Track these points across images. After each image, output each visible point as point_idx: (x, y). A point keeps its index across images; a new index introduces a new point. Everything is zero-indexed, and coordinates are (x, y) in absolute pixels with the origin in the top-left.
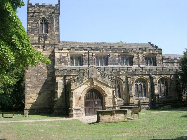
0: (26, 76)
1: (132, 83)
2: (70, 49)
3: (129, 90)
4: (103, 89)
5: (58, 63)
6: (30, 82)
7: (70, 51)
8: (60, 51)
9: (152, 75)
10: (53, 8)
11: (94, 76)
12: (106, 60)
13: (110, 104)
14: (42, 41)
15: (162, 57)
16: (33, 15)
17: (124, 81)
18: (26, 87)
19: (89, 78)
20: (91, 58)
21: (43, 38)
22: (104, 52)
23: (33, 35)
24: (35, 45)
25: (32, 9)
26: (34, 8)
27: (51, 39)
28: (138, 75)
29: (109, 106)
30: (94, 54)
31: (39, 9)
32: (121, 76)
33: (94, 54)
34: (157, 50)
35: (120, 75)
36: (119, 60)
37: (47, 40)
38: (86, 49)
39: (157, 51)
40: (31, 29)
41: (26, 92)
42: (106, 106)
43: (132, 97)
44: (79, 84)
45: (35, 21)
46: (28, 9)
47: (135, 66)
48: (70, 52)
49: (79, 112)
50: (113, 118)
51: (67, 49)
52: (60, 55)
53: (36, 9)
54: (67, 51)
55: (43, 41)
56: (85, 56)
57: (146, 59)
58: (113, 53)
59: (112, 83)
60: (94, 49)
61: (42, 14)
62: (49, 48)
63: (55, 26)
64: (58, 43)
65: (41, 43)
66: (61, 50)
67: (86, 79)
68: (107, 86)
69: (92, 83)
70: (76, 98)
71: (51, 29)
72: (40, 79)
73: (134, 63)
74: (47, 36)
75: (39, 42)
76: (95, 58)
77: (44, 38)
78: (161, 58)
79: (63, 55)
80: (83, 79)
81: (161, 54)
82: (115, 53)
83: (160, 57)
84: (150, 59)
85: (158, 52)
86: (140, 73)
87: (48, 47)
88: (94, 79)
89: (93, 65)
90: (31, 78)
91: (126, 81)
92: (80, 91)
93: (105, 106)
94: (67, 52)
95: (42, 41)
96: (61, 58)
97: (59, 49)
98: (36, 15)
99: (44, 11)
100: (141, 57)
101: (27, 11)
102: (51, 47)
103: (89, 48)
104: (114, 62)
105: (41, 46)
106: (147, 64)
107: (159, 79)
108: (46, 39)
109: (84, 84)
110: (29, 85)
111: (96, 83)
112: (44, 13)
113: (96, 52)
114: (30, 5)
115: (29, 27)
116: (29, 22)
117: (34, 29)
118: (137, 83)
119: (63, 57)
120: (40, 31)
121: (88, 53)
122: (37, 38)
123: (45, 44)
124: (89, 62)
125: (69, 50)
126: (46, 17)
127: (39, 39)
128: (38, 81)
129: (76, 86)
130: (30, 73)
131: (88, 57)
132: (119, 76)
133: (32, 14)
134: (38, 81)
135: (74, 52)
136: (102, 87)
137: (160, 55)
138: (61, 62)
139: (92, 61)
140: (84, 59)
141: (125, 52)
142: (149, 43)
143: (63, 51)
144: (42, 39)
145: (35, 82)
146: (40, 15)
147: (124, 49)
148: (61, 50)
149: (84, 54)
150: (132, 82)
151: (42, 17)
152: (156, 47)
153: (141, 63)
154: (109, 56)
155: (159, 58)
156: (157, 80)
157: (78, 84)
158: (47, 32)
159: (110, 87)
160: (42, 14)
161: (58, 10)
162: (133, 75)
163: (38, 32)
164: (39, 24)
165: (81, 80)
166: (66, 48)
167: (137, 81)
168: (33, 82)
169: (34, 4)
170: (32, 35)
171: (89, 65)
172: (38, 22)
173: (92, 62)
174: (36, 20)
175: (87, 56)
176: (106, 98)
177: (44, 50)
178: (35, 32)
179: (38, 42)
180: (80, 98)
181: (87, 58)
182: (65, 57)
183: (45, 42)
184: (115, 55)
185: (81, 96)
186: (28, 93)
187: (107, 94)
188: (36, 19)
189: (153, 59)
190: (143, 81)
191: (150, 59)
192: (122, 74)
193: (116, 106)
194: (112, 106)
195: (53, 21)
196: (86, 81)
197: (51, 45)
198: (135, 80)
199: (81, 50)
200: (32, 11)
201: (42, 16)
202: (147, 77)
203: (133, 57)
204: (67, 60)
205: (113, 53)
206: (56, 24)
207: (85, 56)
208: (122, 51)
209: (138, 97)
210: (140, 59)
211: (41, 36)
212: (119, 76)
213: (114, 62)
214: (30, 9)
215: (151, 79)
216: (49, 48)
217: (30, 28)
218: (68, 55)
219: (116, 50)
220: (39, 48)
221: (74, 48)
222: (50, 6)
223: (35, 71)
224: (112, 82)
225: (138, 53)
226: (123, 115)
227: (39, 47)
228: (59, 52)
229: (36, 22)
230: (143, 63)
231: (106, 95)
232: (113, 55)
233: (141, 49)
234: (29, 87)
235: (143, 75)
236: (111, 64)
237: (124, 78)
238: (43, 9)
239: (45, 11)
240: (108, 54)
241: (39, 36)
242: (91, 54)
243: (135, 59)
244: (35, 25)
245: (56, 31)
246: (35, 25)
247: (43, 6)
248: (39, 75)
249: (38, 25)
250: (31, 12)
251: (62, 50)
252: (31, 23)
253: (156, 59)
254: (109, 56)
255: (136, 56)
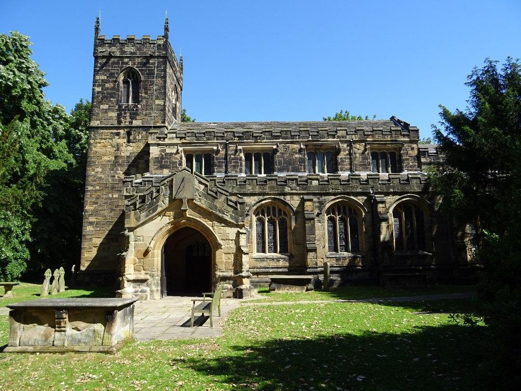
0: (86, 199)
1: (318, 215)
2: (184, 136)
3: (307, 232)
4: (211, 228)
5: (157, 169)
6: (95, 213)
7: (185, 141)
8: (160, 142)
9: (376, 193)
10: (152, 45)
11: (185, 195)
12: (268, 160)
13: (227, 270)
14: (126, 122)
15: (419, 149)
16: (106, 63)
17: (295, 209)
18: (84, 224)
19: (172, 200)
20: (233, 156)
21: (128, 114)
22: (265, 141)
23: (106, 107)
24: (109, 131)
25: (104, 50)
26: (110, 47)
27: (146, 115)
28: (335, 194)
29: (225, 274)
30: (240, 147)
31: (121, 49)
32: (288, 197)
33: (240, 147)
34: (403, 133)
35: (285, 194)
36: (302, 161)
37: (138, 117)
38: (222, 135)
39: (404, 136)
40: (102, 94)
41: (85, 235)
42: (218, 273)
43: (315, 250)
44: (147, 216)
45: (112, 75)
46: (95, 49)
47: (344, 175)
48: (183, 143)
49: (143, 287)
50: (57, 334)
51: (177, 137)
52: (160, 151)
53: (113, 49)
54: (177, 141)
55: (128, 119)
56: (218, 152)
57: (375, 156)
58: (288, 143)
59: (236, 214)
60: (241, 135)
61: (126, 60)
62: (140, 136)
63: (156, 85)
64: (162, 125)
65: (122, 125)
66: (162, 139)
67: (164, 203)
68: (221, 221)
69: (180, 214)
70: (137, 252)
71: (146, 93)
72: (117, 206)
73: (340, 167)
74: (137, 110)
75: (119, 122)
76: (242, 155)
77: (131, 114)
78: (416, 152)
79: (168, 151)
80: (158, 201)
81: (416, 142)
82: (291, 143)
83: (413, 149)
84: (384, 156)
85: (408, 136)
86: (340, 190)
87: (139, 133)
88: (185, 201)
89: (236, 172)
90: (96, 203)
91: (300, 209)
92: (150, 235)
93: (215, 275)
94: (177, 144)
95: (126, 122)
96: (162, 158)
97: (157, 138)
98: (113, 63)
99: (131, 53)
100: (361, 151)
101: (94, 53)
102: (144, 133)
103: (229, 133)
104: (290, 165)
105: (122, 131)
106: (376, 169)
107: (395, 205)
108: (134, 116)
109: (159, 214)
110: (92, 219)
111: (190, 214)
112: (132, 57)
113: (245, 141)
114: (99, 39)
115: (98, 89)
116: (97, 77)
117: (108, 93)
118: (334, 213)
119: (166, 154)
120: (123, 99)
121: (226, 146)
122: (114, 114)
123: (131, 128)
124: (226, 166)
125: (181, 138)
126: (137, 67)
127: (119, 116)
128: (112, 210)
129: (138, 219)
130: (96, 191)
131: (226, 155)
132: (282, 198)
133: (104, 60)
134: (112, 210)
135: (192, 143)
136: (208, 223)
137: (414, 146)
138: (162, 167)
139: (234, 162)
140: (217, 159)
141: (319, 141)
142: (393, 118)
143: (167, 141)
144: (125, 117)
145: (105, 213)
146: (123, 63)
147: (316, 134)
148: (162, 139)
149: (215, 148)
150: (316, 211)
151: (128, 66)
152: (406, 126)
153: (361, 165)
154: (276, 151)
155: (409, 152)
156: (389, 207)
157: (143, 214)
158: (136, 99)
159: (228, 224)
160: (126, 60)
161: (164, 50)
162: (321, 194)
163: (118, 102)
164: (121, 82)
165: (151, 204)
166: (174, 135)
167: (331, 210)
168: (103, 212)
169: (108, 38)
170: (102, 107)
171: (226, 172)
172: (117, 78)
173: (234, 166)
174: (114, 74)
175: (223, 152)
176: (218, 253)
177: (129, 141)
178: (111, 101)
179: (116, 124)
180: (146, 253)
181: (224, 157)
182: (171, 154)
183: (131, 123)
184: (291, 148)
185: (152, 245)
186: (90, 237)
187: (220, 241)
188: (113, 71)
189: (393, 155)
190: (350, 210)
191: (384, 156)
192: (292, 191)
193: (243, 274)
194: (231, 274)
195: (151, 73)
196: (165, 206)
197: (146, 128)
198: (327, 206)
199: (208, 139)
200: (105, 54)
201: (127, 63)
202: (361, 200)
203: (338, 151)
204: (176, 162)
205: (288, 143)
206: (159, 81)
207: (218, 152)
208: (310, 139)
209: (336, 250)
210: (358, 155)
211: (125, 110)
212: (282, 198)
213: (290, 164)
214: (100, 49)
215: (372, 204)
216: (140, 136)
217: (99, 92)
218: (178, 150)
219: (293, 137)
220: (118, 137)
221: (194, 134)
222: (145, 42)
223: (108, 187)
224: (236, 209)
225: (350, 144)
226: (99, 327)
227: (118, 134)
228: (158, 145)
229: (113, 77)
230: (365, 167)
231: (219, 246)
232: (287, 149)
233: (362, 133)
234: (91, 223)
235: (348, 194)
236: (281, 170)
237: (295, 202)
238: (129, 49)
239: (134, 53)
240: (275, 147)
241: (120, 108)
242: (232, 147)
243: (342, 156)
244: (112, 85)
245: (157, 98)
246: (112, 85)
247: (131, 40)
248: (116, 196)
249: (118, 85)
250: (103, 57)
251: (164, 138)
252: (102, 80)
253: (400, 156)
254: (276, 151)
255: (345, 150)
